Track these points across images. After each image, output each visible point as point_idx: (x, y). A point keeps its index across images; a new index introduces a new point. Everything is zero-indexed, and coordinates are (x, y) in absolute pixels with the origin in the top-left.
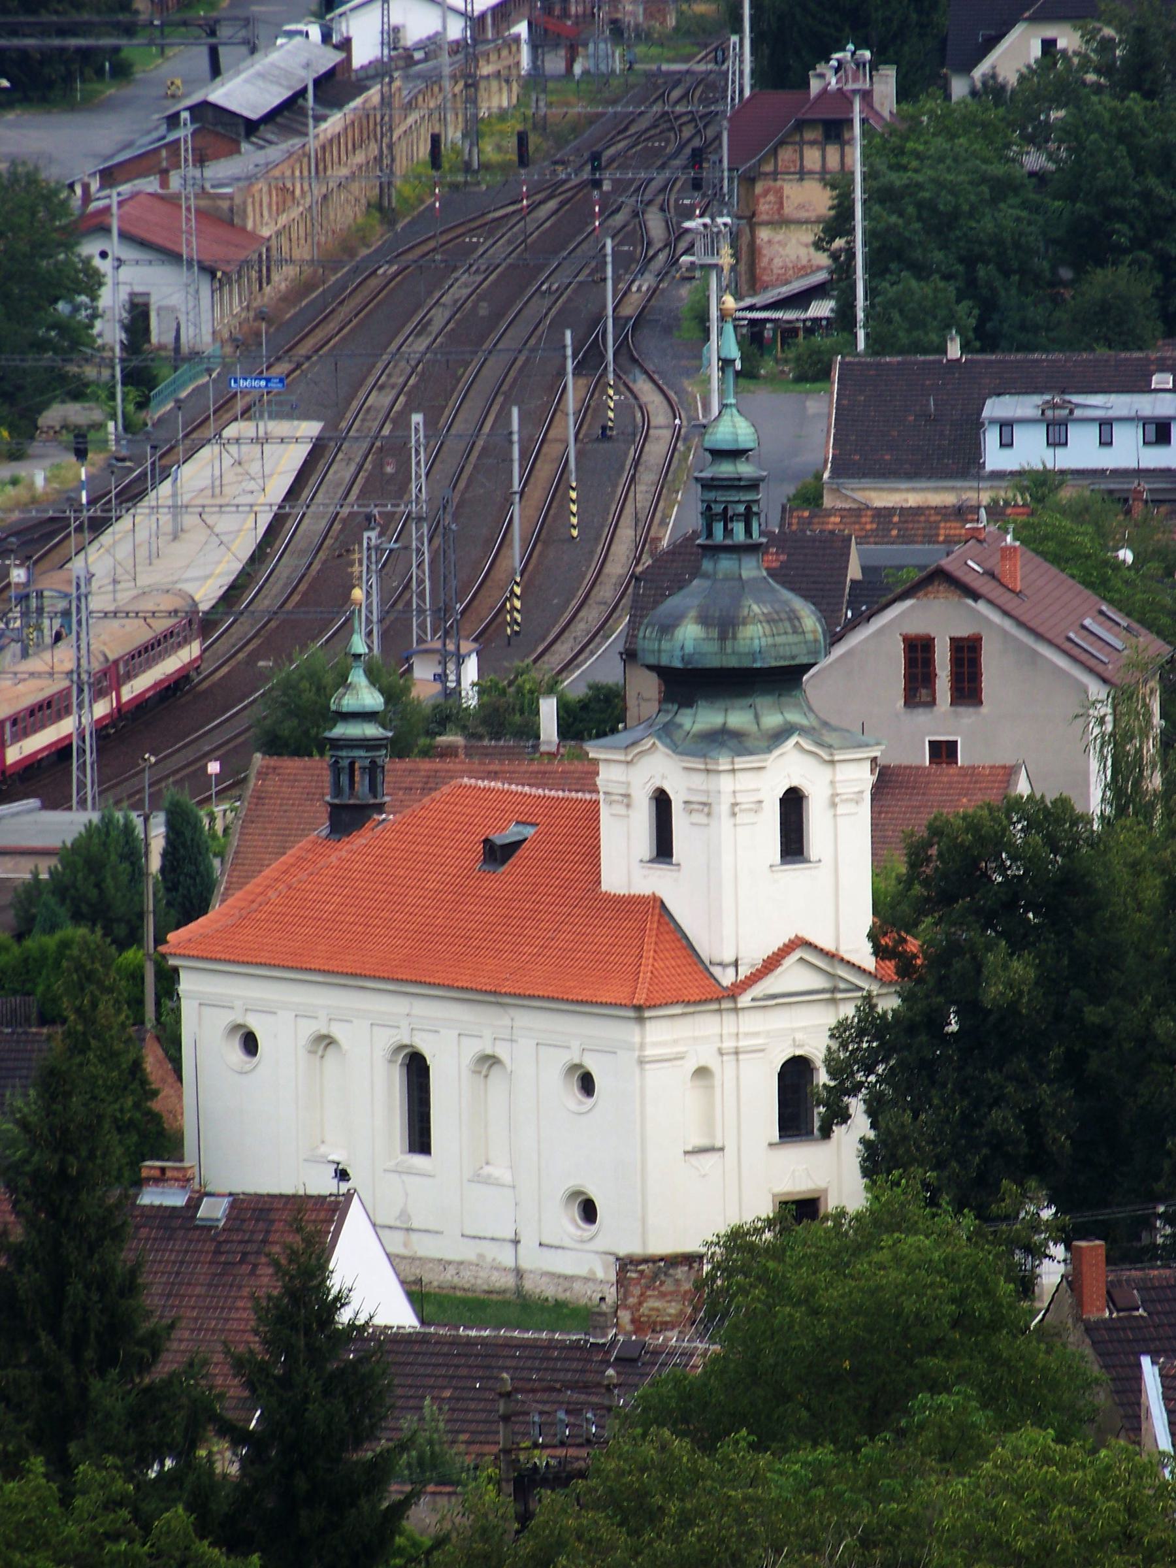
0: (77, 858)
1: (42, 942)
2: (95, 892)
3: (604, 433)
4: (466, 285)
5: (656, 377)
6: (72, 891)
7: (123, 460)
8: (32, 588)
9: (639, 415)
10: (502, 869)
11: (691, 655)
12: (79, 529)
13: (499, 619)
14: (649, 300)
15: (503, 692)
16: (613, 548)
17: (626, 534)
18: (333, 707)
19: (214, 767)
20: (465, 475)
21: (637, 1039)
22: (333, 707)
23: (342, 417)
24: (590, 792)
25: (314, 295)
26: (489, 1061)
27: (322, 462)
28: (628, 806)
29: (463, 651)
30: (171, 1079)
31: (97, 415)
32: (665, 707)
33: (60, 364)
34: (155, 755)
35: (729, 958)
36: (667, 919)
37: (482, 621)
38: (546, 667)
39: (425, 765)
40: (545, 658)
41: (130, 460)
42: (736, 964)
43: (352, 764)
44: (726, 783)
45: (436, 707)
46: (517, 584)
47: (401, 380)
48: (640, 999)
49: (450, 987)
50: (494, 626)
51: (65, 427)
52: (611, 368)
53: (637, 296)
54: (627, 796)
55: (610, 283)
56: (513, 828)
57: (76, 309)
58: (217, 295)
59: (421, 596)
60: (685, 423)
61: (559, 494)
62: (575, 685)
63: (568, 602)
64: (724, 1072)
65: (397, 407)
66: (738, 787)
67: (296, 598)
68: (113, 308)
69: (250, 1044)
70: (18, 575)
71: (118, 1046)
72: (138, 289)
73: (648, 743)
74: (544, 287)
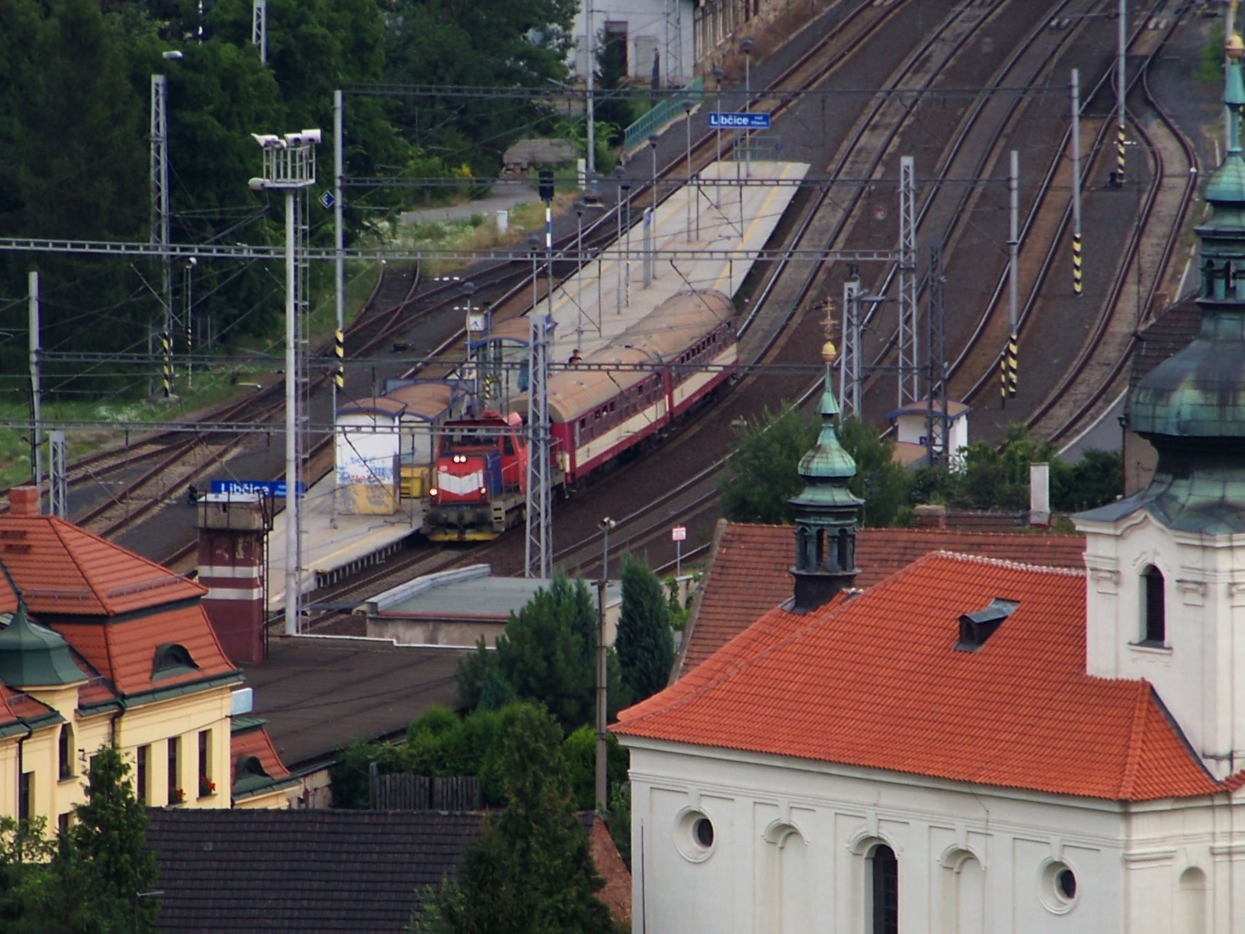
0: (525, 629)
1: (486, 717)
2: (544, 664)
3: (1113, 180)
4: (967, 19)
5: (1171, 121)
6: (520, 665)
7: (593, 201)
8: (490, 337)
9: (1151, 163)
10: (980, 649)
11: (1187, 422)
12: (543, 275)
13: (994, 380)
14: (1166, 39)
15: (993, 459)
16: (1120, 305)
17: (1128, 306)
18: (801, 471)
19: (679, 533)
20: (961, 225)
21: (1122, 836)
22: (801, 471)
23: (830, 159)
24: (1077, 567)
25: (805, 27)
26: (962, 856)
27: (808, 206)
28: (1117, 583)
29: (951, 413)
30: (620, 869)
31: (567, 152)
32: (1158, 478)
33: (526, 96)
34: (616, 520)
35: (1223, 750)
36: (1157, 706)
37: (974, 381)
38: (1044, 431)
39: (904, 535)
40: (1042, 423)
41: (601, 202)
42: (1231, 757)
43: (820, 532)
44: (1224, 562)
45: (920, 472)
46: (1014, 342)
47: (896, 120)
48: (1126, 793)
49: (922, 776)
50: (987, 387)
51: (532, 164)
52: (1122, 112)
53: (1155, 32)
54: (1117, 573)
55: (1122, 21)
56: (992, 605)
57: (548, 37)
58: (700, 26)
59: (909, 353)
60: (1201, 172)
61: (1062, 246)
62: (1070, 452)
63: (1069, 362)
64: (1216, 874)
65: (890, 149)
66: (1237, 566)
67: (774, 352)
68: (586, 37)
69: (705, 832)
70: (475, 322)
71: (562, 832)
72: (614, 17)
73: (1139, 516)
74: (1054, 23)
